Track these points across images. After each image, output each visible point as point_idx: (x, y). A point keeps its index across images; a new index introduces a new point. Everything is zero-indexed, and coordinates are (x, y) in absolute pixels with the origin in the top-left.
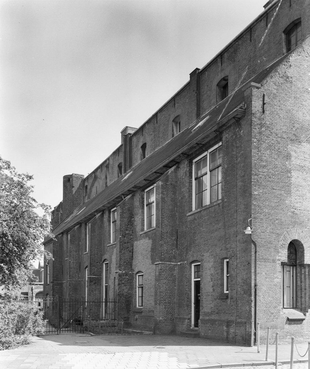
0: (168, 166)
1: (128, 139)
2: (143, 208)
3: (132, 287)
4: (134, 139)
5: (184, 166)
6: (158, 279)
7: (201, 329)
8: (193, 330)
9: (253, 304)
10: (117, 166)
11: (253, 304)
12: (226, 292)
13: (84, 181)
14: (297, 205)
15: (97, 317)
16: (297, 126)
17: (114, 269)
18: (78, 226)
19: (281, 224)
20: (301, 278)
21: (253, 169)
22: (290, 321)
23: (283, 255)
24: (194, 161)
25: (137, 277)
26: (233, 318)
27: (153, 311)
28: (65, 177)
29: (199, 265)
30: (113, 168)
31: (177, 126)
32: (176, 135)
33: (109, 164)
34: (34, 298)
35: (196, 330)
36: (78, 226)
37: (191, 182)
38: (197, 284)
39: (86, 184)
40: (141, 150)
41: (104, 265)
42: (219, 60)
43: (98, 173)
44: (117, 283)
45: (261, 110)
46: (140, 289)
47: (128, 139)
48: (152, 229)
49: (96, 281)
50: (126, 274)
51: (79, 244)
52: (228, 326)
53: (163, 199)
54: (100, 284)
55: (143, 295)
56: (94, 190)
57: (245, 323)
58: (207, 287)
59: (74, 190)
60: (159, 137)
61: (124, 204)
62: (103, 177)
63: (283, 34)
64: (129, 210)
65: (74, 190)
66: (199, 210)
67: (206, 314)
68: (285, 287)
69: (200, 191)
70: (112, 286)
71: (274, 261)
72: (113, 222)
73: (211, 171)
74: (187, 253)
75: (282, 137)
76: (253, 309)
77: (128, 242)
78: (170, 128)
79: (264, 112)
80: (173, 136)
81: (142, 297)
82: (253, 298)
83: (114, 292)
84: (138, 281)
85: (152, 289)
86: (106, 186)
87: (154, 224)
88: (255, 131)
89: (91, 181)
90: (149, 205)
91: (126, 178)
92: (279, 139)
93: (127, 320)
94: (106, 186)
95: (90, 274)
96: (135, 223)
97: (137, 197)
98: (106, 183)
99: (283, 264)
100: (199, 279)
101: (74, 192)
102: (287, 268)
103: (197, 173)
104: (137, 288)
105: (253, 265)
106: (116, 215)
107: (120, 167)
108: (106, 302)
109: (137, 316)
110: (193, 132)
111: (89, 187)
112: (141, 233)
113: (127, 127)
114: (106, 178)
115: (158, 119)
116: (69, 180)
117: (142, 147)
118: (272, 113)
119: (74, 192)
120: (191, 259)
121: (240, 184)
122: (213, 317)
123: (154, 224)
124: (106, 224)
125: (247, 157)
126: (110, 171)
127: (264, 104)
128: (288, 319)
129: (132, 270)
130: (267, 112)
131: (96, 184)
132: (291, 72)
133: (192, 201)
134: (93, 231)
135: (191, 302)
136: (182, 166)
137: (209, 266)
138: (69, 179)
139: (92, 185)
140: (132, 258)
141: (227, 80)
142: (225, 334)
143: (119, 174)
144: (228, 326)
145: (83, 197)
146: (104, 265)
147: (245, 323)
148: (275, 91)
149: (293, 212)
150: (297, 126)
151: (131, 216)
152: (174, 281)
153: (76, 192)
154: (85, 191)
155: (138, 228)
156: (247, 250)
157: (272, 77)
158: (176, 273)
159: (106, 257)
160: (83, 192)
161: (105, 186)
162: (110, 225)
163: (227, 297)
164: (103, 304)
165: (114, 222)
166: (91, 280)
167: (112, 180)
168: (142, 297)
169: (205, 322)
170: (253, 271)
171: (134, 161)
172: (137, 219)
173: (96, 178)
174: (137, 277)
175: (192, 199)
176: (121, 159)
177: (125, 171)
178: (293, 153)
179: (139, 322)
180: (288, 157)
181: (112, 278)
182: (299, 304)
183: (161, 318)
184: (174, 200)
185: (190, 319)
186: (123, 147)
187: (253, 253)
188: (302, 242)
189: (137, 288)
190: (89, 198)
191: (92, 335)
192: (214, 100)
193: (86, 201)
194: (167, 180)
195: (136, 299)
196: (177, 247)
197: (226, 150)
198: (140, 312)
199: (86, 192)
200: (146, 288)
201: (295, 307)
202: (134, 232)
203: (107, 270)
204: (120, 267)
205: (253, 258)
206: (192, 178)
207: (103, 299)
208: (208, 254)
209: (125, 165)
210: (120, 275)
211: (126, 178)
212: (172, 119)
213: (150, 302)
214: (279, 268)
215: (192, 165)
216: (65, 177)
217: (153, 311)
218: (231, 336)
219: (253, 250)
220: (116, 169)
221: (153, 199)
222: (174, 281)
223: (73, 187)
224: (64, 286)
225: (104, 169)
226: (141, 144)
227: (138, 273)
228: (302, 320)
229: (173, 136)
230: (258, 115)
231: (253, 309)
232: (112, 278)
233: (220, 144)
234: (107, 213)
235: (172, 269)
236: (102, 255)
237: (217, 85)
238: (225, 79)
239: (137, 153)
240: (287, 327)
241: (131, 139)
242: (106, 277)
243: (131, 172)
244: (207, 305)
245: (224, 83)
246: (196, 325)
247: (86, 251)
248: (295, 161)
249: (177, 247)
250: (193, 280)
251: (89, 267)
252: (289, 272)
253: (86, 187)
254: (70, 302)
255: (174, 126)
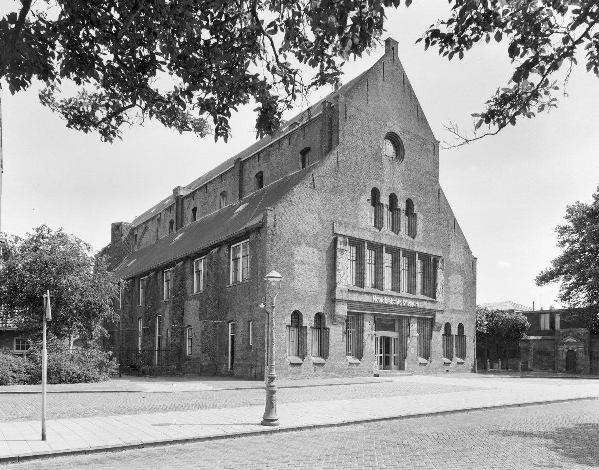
0: (213, 247)
1: (180, 200)
2: (193, 274)
3: (183, 339)
4: (186, 201)
5: (224, 249)
6: (203, 334)
7: (235, 371)
8: (229, 372)
9: (266, 353)
10: (168, 221)
11: (266, 353)
12: (251, 344)
13: (133, 230)
14: (299, 287)
15: (151, 363)
16: (298, 234)
17: (167, 324)
18: (131, 280)
19: (286, 300)
20: (301, 336)
21: (268, 264)
22: (292, 365)
23: (288, 321)
24: (232, 246)
25: (187, 330)
26: (254, 363)
27: (200, 358)
28: (113, 225)
29: (234, 324)
30: (164, 223)
31: (224, 199)
32: (222, 208)
33: (160, 218)
34: (494, 370)
35: (231, 372)
36: (131, 280)
37: (229, 262)
38: (233, 338)
39: (136, 233)
40: (191, 213)
41: (157, 318)
42: (257, 157)
43: (149, 224)
44: (169, 335)
45: (273, 225)
46: (190, 340)
47: (180, 200)
48: (200, 293)
49: (149, 333)
50: (178, 328)
51: (132, 297)
52: (251, 368)
53: (208, 272)
54: (154, 335)
55: (193, 346)
56: (144, 240)
57: (261, 366)
58: (239, 341)
59: (123, 238)
60: (208, 205)
61: (177, 269)
62: (155, 230)
63: (300, 154)
64: (181, 274)
65: (123, 238)
66: (234, 284)
67: (238, 360)
68: (290, 341)
69: (236, 270)
70: (165, 337)
71: (281, 324)
72: (166, 281)
73: (243, 257)
74: (226, 315)
75: (287, 242)
76: (266, 356)
77: (180, 301)
78: (218, 200)
79: (275, 226)
80: (220, 208)
81: (191, 346)
82: (266, 348)
83: (167, 342)
84: (188, 334)
85: (199, 341)
86: (158, 239)
87: (201, 288)
88: (269, 238)
89: (141, 231)
90: (198, 272)
91: (177, 238)
92: (285, 244)
93: (178, 365)
94: (158, 239)
95: (144, 325)
96: (186, 286)
97: (188, 265)
98: (157, 236)
99: (288, 326)
100: (234, 335)
101: (123, 240)
102: (291, 329)
103: (234, 255)
104: (187, 340)
105: (266, 327)
106: (169, 274)
107: (171, 223)
108: (159, 351)
109: (187, 363)
110: (235, 215)
111: (139, 237)
112: (191, 295)
113: (179, 187)
114: (157, 231)
115: (208, 189)
116: (118, 228)
117: (193, 210)
118: (280, 226)
119: (123, 240)
120: (229, 320)
121: (259, 272)
122: (242, 362)
123: (201, 288)
124: (160, 282)
125: (263, 255)
126: (162, 225)
127: (275, 221)
128: (291, 363)
129: (183, 324)
130: (277, 226)
131: (146, 235)
132: (293, 199)
133: (230, 276)
134: (147, 288)
135: (228, 351)
136: (223, 249)
137: (240, 325)
138: (118, 227)
139: (143, 235)
140: (183, 314)
141: (262, 173)
142: (249, 374)
143: (171, 230)
144: (251, 368)
145: (133, 245)
146: (157, 318)
147: (261, 366)
148: (283, 212)
149: (295, 292)
150: (298, 234)
151: (183, 279)
152: (216, 335)
153: (125, 240)
154: (134, 240)
155: (189, 290)
156: (262, 317)
157: (281, 203)
158: (217, 329)
159: (160, 311)
160: (133, 241)
161: (156, 238)
162: (163, 283)
163: (251, 348)
164: (155, 353)
165: (167, 281)
166: (144, 331)
167: (163, 235)
168: (191, 346)
169: (237, 366)
170: (266, 331)
171: (185, 221)
172: (188, 282)
173: (146, 229)
174: (187, 330)
175: (230, 274)
176: (172, 216)
177: (177, 229)
178: (295, 252)
179: (188, 367)
180: (292, 255)
181: (165, 330)
182: (299, 353)
183: (205, 364)
184: (217, 274)
185: (227, 364)
186: (175, 205)
187: (266, 319)
188: (302, 312)
189: (187, 340)
190: (138, 247)
191: (150, 377)
192: (252, 188)
193: (136, 250)
194: (211, 259)
195: (186, 349)
196: (218, 309)
197: (252, 245)
198: (189, 359)
199: (136, 240)
200: (194, 339)
201: (298, 356)
202: (185, 293)
203: (160, 323)
204: (172, 322)
205: (266, 322)
206: (230, 258)
207: (155, 349)
208: (239, 317)
209: (177, 223)
210: (173, 329)
211: (177, 238)
212: (219, 193)
213: (197, 351)
214: (284, 329)
215: (230, 249)
216: (113, 225)
217: (200, 358)
218: (252, 375)
219: (266, 317)
220: (168, 225)
221: (201, 267)
222: (216, 335)
223: (122, 235)
224: (115, 335)
225: (156, 222)
226: (192, 208)
227: (188, 326)
228: (301, 364)
229: (220, 208)
230: (271, 228)
231: (266, 356)
232: (165, 330)
233: (248, 240)
234: (161, 272)
235: (215, 326)
236: (155, 309)
237: (256, 176)
238: (261, 173)
239: (188, 215)
240: (290, 368)
241: (182, 200)
242: (159, 329)
243: (183, 234)
244: (239, 354)
245: (260, 175)
246: (231, 369)
247: (139, 304)
248: (297, 257)
249: (218, 309)
250: (230, 335)
251: (143, 318)
252: (293, 333)
253: (136, 236)
254: (70, 349)
255: (221, 199)
